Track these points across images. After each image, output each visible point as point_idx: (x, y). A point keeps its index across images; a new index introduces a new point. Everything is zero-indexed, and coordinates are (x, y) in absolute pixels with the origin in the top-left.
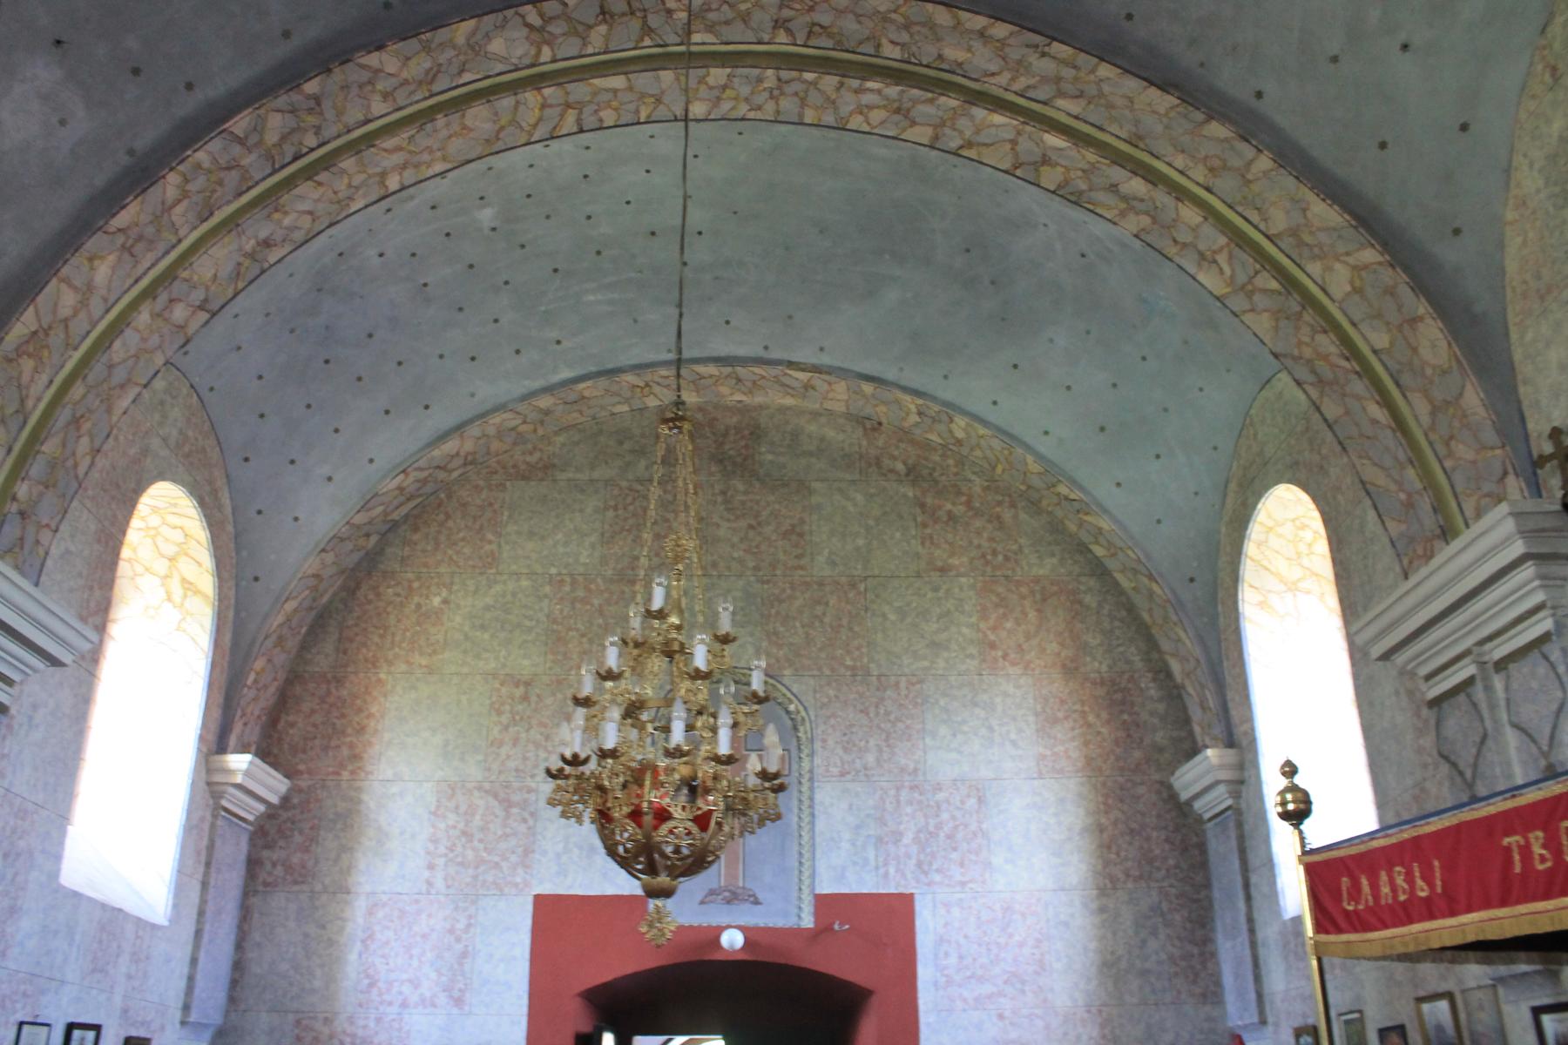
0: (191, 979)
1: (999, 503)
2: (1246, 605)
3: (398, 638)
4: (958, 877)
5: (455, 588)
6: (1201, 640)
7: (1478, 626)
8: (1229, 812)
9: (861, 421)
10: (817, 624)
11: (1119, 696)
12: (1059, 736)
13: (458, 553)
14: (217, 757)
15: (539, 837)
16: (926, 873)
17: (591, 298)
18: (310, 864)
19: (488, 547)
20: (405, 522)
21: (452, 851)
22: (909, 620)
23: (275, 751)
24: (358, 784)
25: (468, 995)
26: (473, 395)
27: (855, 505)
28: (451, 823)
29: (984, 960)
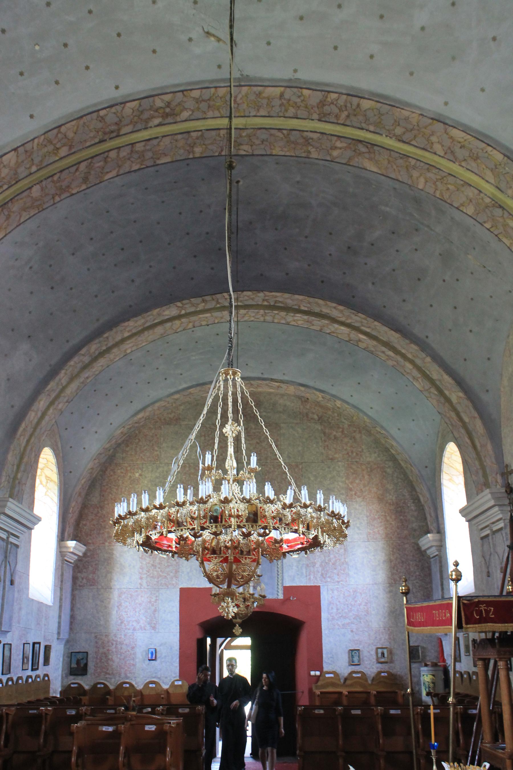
0: (59, 623)
1: (355, 432)
2: (444, 480)
3: (123, 490)
4: (337, 579)
5: (144, 469)
6: (429, 490)
7: (493, 517)
8: (437, 557)
9: (300, 398)
10: (283, 482)
11: (399, 509)
12: (376, 525)
13: (144, 455)
14: (63, 542)
15: (181, 566)
16: (325, 578)
17: (194, 358)
18: (96, 578)
19: (156, 453)
20: (123, 443)
21: (148, 572)
22: (319, 480)
23: (80, 535)
24: (112, 547)
25: (157, 625)
26: (149, 396)
27: (298, 433)
28: (147, 561)
29: (346, 610)
